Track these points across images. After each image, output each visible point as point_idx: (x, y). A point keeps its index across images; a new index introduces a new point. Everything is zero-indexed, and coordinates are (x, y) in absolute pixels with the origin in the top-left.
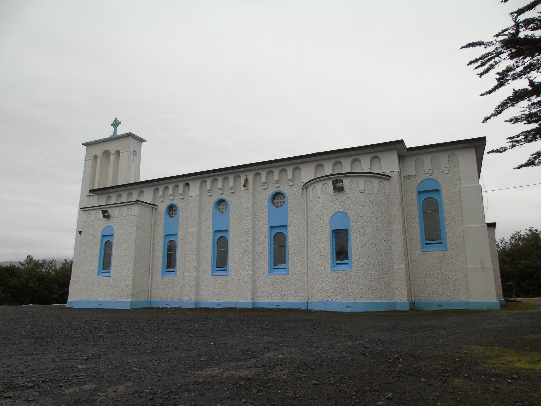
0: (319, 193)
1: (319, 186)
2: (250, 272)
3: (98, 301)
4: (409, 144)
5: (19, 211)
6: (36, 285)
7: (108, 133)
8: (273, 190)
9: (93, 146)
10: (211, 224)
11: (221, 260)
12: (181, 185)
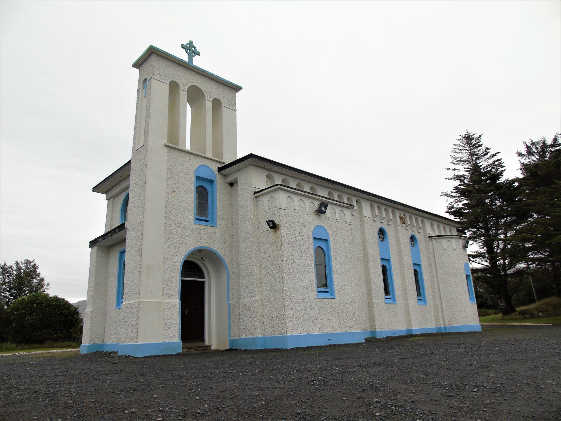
7: (183, 56)
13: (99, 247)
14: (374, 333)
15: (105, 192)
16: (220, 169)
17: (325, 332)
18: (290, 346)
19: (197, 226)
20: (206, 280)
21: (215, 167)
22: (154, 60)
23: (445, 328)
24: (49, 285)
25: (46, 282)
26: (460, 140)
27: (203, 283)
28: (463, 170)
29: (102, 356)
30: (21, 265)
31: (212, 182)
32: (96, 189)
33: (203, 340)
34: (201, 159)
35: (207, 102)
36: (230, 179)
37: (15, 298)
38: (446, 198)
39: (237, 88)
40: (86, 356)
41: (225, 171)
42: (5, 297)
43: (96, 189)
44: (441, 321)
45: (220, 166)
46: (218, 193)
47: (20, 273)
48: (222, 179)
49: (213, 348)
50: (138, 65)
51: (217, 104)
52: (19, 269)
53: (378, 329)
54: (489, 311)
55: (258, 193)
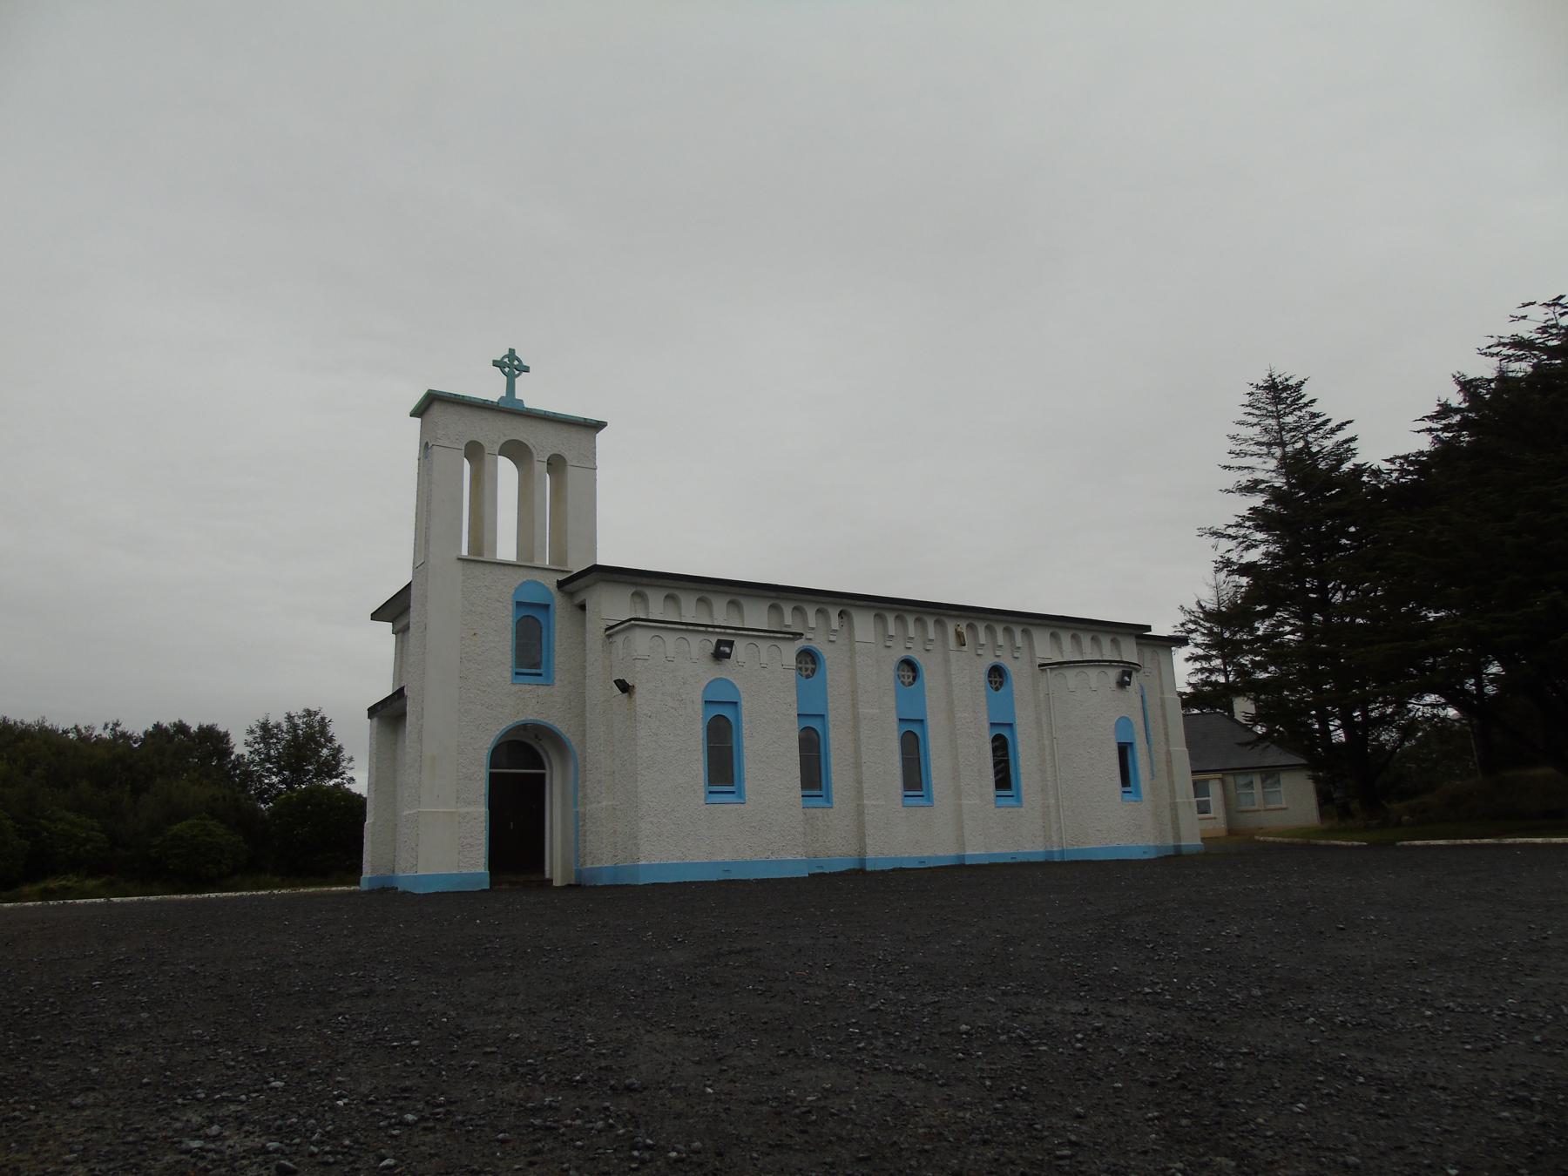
0: (764, 658)
1: (1093, 674)
2: (964, 802)
3: (717, 864)
4: (1156, 631)
5: (207, 556)
6: (217, 819)
7: (491, 388)
8: (989, 661)
9: (486, 415)
10: (893, 704)
11: (914, 777)
12: (834, 614)
13: (380, 718)
14: (862, 861)
15: (393, 620)
16: (560, 584)
17: (719, 859)
18: (643, 880)
19: (517, 688)
20: (547, 772)
21: (550, 581)
22: (436, 409)
23: (1062, 852)
24: (351, 759)
25: (346, 754)
26: (1251, 394)
27: (543, 776)
28: (1266, 469)
29: (387, 893)
30: (297, 721)
31: (547, 607)
32: (377, 616)
33: (543, 872)
34: (525, 572)
35: (536, 464)
36: (578, 600)
37: (290, 787)
38: (1213, 540)
39: (599, 426)
40: (370, 892)
41: (569, 587)
42: (272, 785)
43: (377, 616)
44: (1055, 838)
45: (562, 577)
46: (558, 627)
47: (296, 736)
48: (568, 601)
49: (557, 883)
50: (416, 413)
51: (556, 464)
52: (295, 727)
53: (870, 854)
54: (91, 883)
55: (611, 631)
